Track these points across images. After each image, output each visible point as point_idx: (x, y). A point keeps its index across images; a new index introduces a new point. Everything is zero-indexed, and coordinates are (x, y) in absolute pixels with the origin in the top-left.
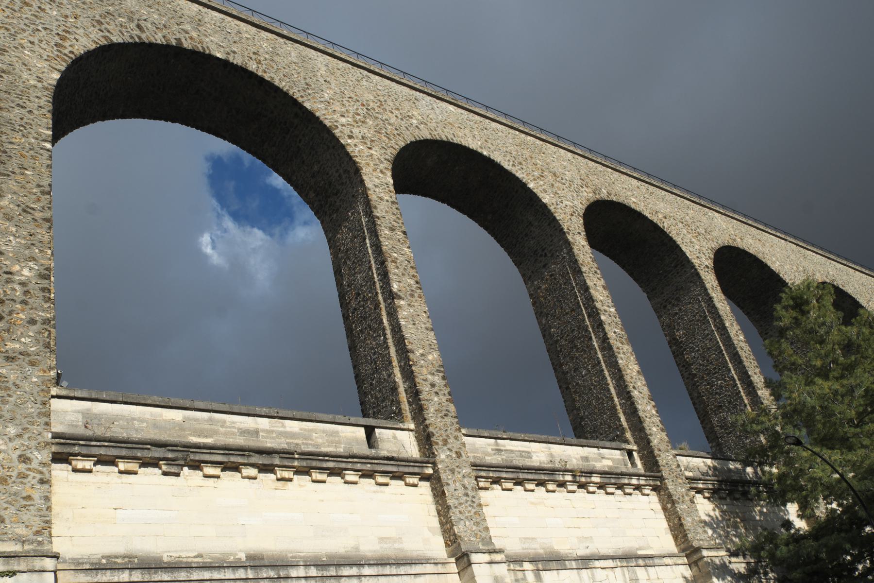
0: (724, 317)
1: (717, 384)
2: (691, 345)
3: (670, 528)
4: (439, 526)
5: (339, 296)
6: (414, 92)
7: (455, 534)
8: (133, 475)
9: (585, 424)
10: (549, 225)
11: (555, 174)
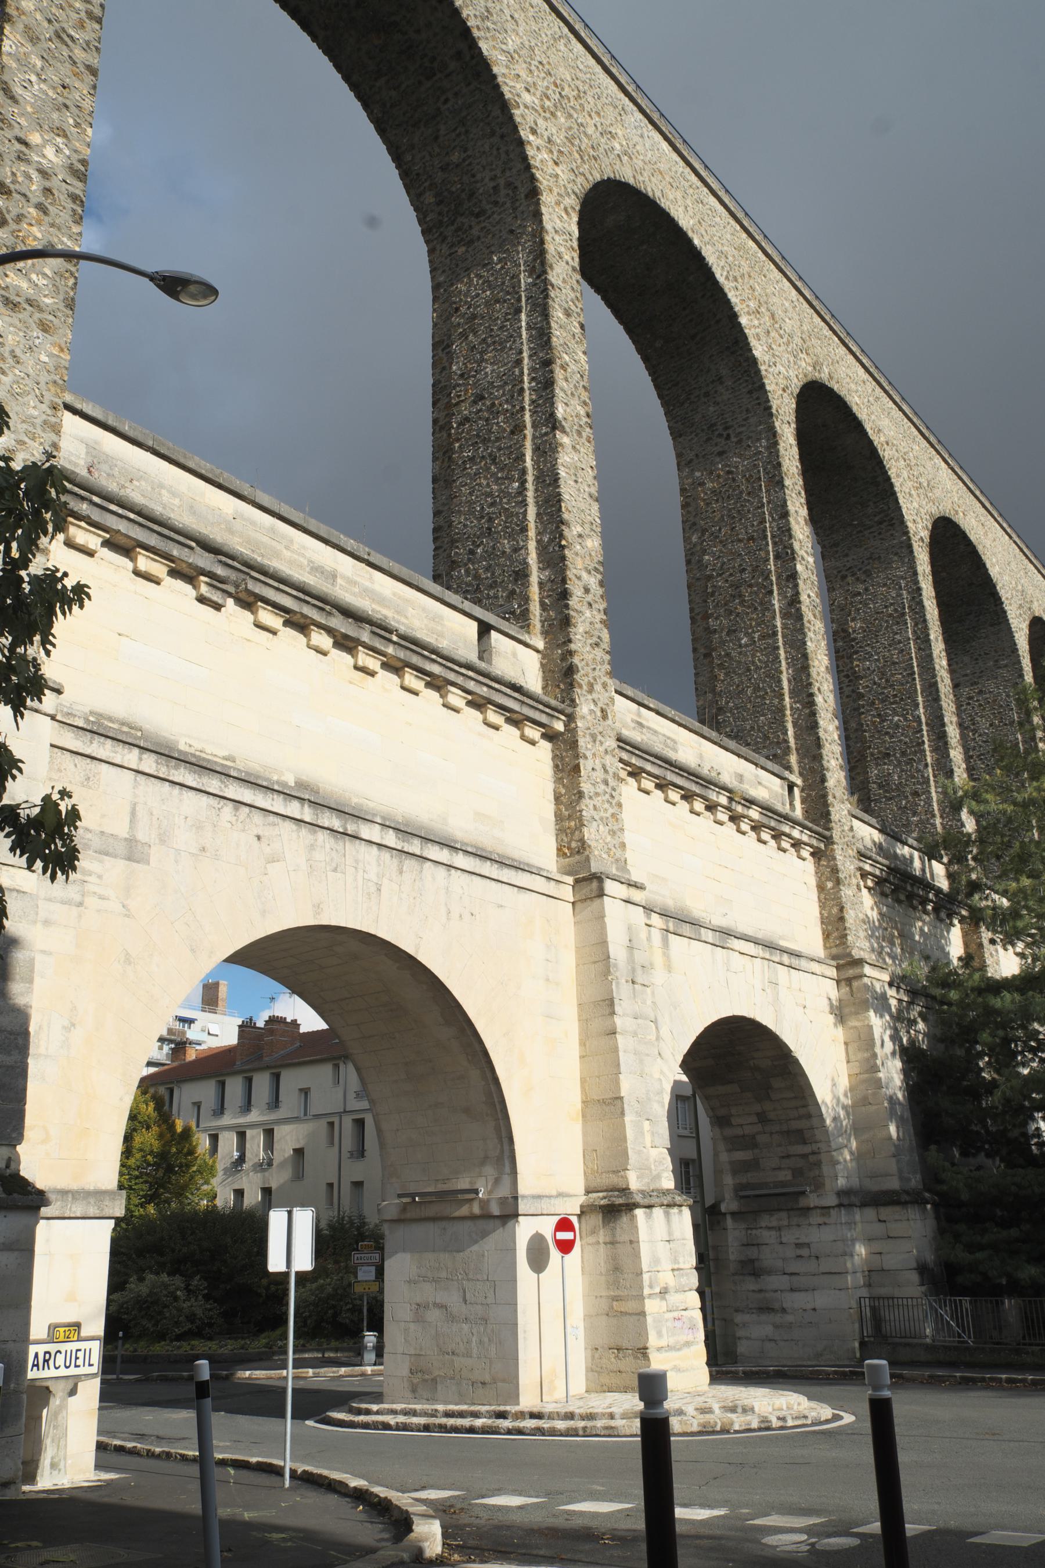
0: (930, 625)
1: (891, 721)
2: (868, 649)
3: (822, 918)
4: (554, 819)
5: (433, 385)
6: (621, 96)
7: (582, 841)
8: (153, 585)
9: (724, 721)
10: (750, 392)
11: (773, 316)
